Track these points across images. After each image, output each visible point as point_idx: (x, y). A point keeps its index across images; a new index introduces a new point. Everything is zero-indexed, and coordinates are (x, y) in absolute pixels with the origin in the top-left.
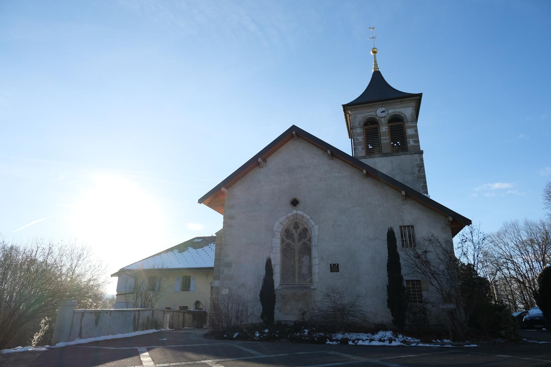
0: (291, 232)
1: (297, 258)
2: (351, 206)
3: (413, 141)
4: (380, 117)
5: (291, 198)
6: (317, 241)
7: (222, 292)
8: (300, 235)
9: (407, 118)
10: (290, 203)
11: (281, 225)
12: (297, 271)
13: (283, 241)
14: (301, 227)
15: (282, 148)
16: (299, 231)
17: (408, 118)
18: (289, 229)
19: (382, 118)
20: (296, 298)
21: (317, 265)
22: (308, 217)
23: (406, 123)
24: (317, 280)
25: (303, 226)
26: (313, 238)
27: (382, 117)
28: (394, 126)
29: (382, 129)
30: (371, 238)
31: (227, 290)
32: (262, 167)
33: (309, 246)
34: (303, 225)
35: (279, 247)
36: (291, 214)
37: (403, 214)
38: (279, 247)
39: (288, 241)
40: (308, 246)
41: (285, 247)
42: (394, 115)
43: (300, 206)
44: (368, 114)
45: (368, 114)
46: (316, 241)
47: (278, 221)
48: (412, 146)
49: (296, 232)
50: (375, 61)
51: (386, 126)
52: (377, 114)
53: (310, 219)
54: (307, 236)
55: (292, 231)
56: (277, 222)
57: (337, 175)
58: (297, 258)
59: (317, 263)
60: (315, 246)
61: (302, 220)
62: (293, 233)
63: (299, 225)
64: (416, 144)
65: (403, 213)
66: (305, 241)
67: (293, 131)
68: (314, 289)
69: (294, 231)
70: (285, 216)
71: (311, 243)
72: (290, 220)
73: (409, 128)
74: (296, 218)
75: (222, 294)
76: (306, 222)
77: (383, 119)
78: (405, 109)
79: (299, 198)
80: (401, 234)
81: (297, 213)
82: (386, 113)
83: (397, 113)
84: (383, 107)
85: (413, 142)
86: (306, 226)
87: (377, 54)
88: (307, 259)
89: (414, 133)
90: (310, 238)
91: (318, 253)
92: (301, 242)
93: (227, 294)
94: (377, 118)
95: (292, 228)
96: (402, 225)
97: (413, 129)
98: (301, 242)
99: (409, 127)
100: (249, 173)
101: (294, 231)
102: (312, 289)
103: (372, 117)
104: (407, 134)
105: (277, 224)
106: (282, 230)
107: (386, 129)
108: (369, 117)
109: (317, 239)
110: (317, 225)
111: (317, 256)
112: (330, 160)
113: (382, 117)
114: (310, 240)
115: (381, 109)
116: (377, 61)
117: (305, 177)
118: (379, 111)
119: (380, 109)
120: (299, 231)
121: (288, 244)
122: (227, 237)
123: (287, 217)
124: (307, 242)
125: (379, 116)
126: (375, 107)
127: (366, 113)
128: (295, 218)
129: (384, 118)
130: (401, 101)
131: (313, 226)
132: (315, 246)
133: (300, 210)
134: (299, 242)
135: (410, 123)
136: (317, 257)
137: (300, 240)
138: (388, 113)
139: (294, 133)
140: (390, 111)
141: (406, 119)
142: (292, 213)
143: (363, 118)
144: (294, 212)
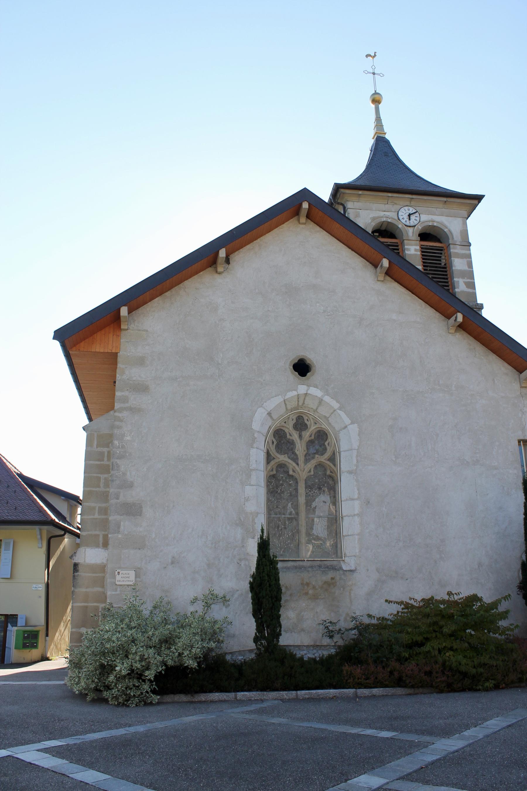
0: (288, 436)
1: (302, 499)
2: (427, 388)
3: (466, 283)
4: (406, 225)
5: (294, 357)
6: (357, 460)
7: (118, 578)
8: (310, 443)
9: (454, 237)
10: (292, 367)
11: (269, 418)
12: (303, 530)
13: (269, 458)
14: (313, 428)
15: (268, 237)
16: (307, 435)
17: (455, 239)
18: (284, 429)
19: (409, 228)
20: (311, 592)
21: (356, 517)
22: (335, 405)
23: (451, 246)
24: (357, 551)
25: (316, 426)
26: (342, 453)
27: (410, 226)
28: (428, 247)
29: (409, 250)
30: (467, 462)
31: (132, 574)
32: (220, 273)
33: (331, 472)
34: (316, 423)
35: (261, 471)
36: (295, 393)
37: (524, 416)
38: (261, 471)
39: (283, 458)
40: (328, 473)
41: (275, 472)
42: (430, 226)
43: (312, 377)
44: (382, 214)
45: (382, 214)
46: (355, 461)
47: (261, 406)
48: (463, 292)
49: (300, 436)
50: (378, 119)
51: (416, 245)
52: (401, 218)
53: (340, 409)
54: (326, 449)
55: (290, 435)
56: (260, 410)
57: (394, 317)
58: (302, 499)
59: (356, 512)
60: (350, 472)
61: (315, 411)
62: (293, 441)
63: (306, 421)
64: (470, 290)
65: (523, 413)
66: (323, 460)
67: (304, 201)
68: (351, 571)
69: (295, 436)
70: (280, 396)
71: (335, 465)
72: (289, 407)
73: (458, 258)
74: (304, 403)
75: (117, 583)
76: (325, 417)
77: (410, 230)
78: (450, 219)
79: (311, 357)
80: (520, 458)
81: (309, 392)
82: (406, 221)
83: (435, 224)
84: (411, 206)
85: (465, 286)
86: (325, 426)
87: (380, 106)
88: (325, 502)
89: (466, 268)
90: (334, 454)
91: (358, 490)
92: (313, 463)
93: (131, 583)
94: (400, 226)
95: (289, 429)
96: (522, 438)
97: (465, 261)
98: (313, 463)
99: (458, 256)
100: (186, 283)
101: (295, 436)
102: (346, 571)
103: (389, 220)
104: (453, 268)
105: (260, 415)
106: (268, 431)
107: (416, 250)
108: (384, 219)
109: (357, 456)
110: (356, 425)
111: (356, 496)
112: (379, 283)
113: (410, 226)
114: (332, 459)
115: (406, 209)
116: (382, 119)
117: (324, 311)
118: (403, 214)
119: (406, 208)
120: (307, 435)
121: (281, 466)
122: (128, 438)
123: (284, 401)
124: (328, 462)
125: (403, 221)
126: (396, 204)
127: (378, 212)
128: (300, 404)
129: (412, 228)
130: (445, 202)
131: (346, 427)
132: (350, 472)
133: (316, 386)
134: (307, 461)
135: (458, 247)
136: (357, 499)
137: (308, 458)
138: (420, 221)
139: (305, 205)
140: (424, 218)
141: (453, 238)
142: (296, 390)
143: (374, 219)
144: (302, 389)
